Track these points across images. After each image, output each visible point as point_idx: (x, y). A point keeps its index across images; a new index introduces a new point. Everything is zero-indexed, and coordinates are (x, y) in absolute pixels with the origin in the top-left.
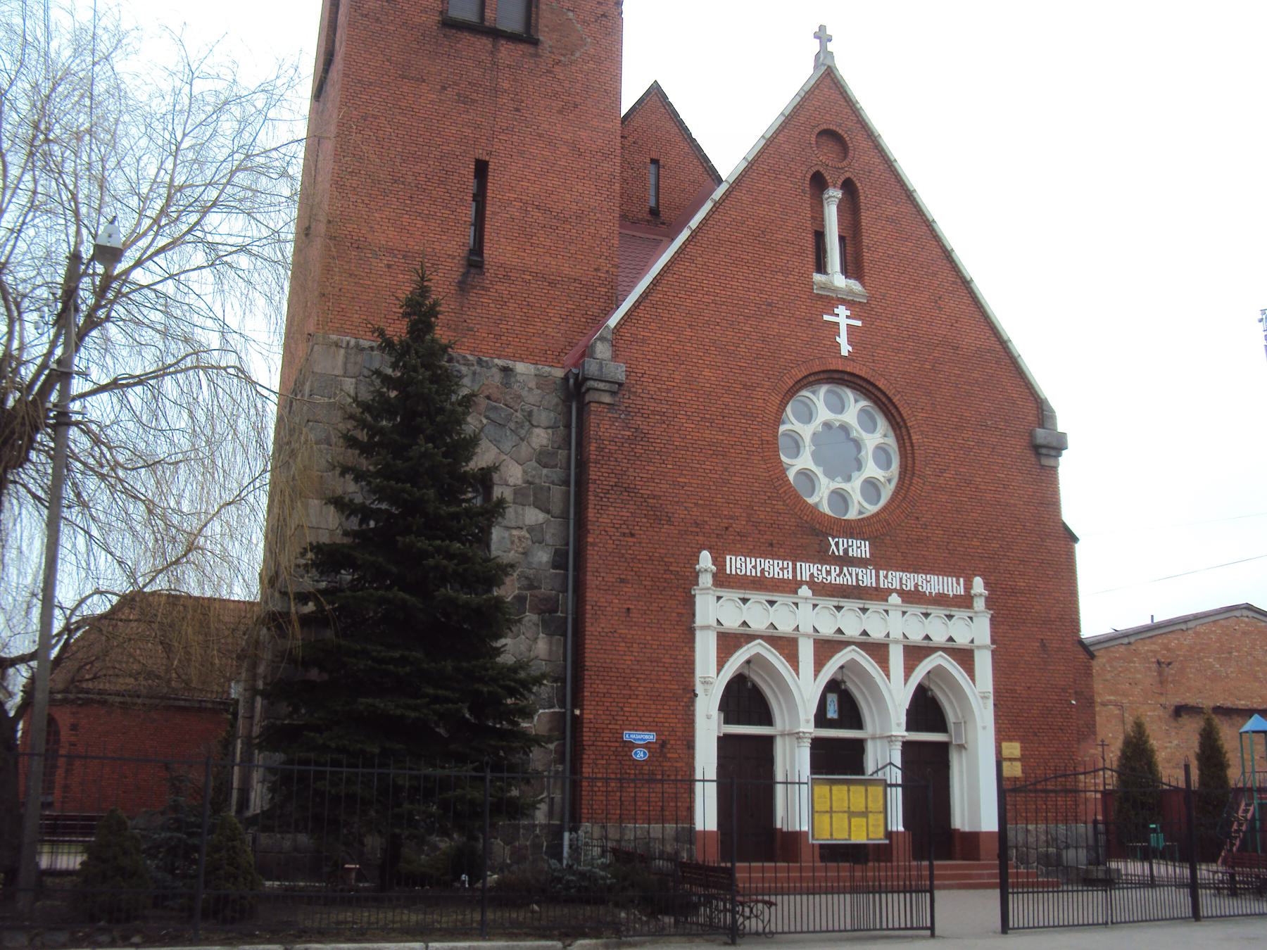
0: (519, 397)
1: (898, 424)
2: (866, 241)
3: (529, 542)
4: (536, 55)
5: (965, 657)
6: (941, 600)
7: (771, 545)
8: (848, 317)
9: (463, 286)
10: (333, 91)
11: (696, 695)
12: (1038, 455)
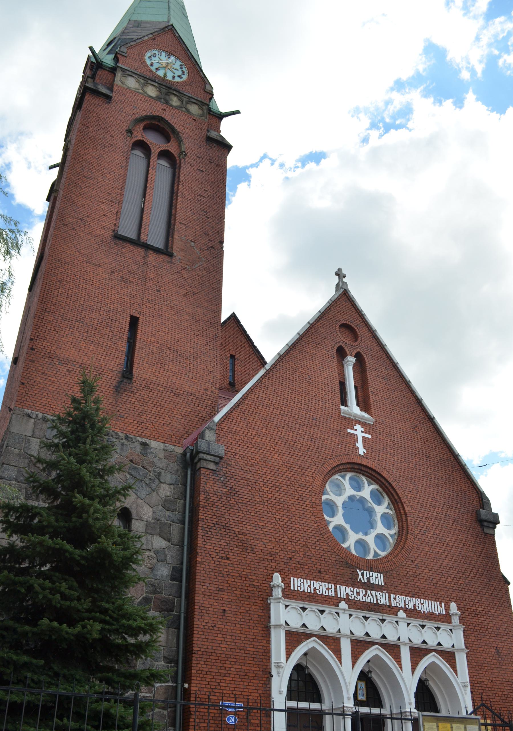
0: (153, 463)
1: (396, 502)
2: (370, 389)
3: (155, 560)
4: (171, 263)
5: (449, 656)
6: (430, 616)
7: (320, 572)
8: (362, 432)
9: (118, 389)
10: (39, 282)
11: (272, 676)
12: (482, 526)
